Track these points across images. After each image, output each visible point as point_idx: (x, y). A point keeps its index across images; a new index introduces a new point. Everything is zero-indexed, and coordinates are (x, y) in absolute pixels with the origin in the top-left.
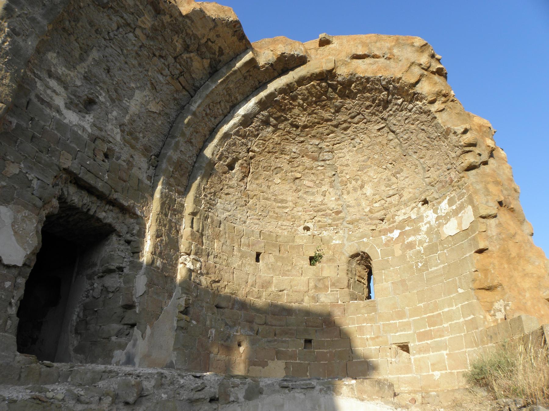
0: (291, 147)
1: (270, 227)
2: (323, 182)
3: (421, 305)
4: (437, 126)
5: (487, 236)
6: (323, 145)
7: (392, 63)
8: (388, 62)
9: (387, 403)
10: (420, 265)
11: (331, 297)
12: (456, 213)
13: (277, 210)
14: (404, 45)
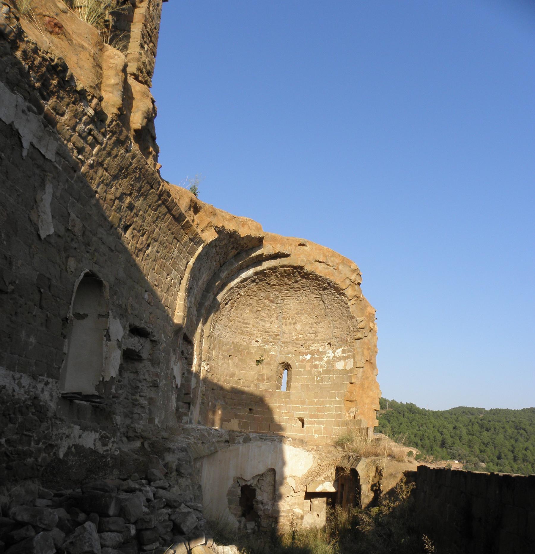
0: (261, 293)
1: (238, 339)
2: (273, 316)
3: (315, 400)
4: (348, 311)
5: (357, 377)
6: (280, 296)
7: (336, 272)
8: (335, 271)
9: (304, 449)
10: (319, 379)
11: (266, 386)
12: (345, 358)
13: (243, 329)
14: (346, 265)
